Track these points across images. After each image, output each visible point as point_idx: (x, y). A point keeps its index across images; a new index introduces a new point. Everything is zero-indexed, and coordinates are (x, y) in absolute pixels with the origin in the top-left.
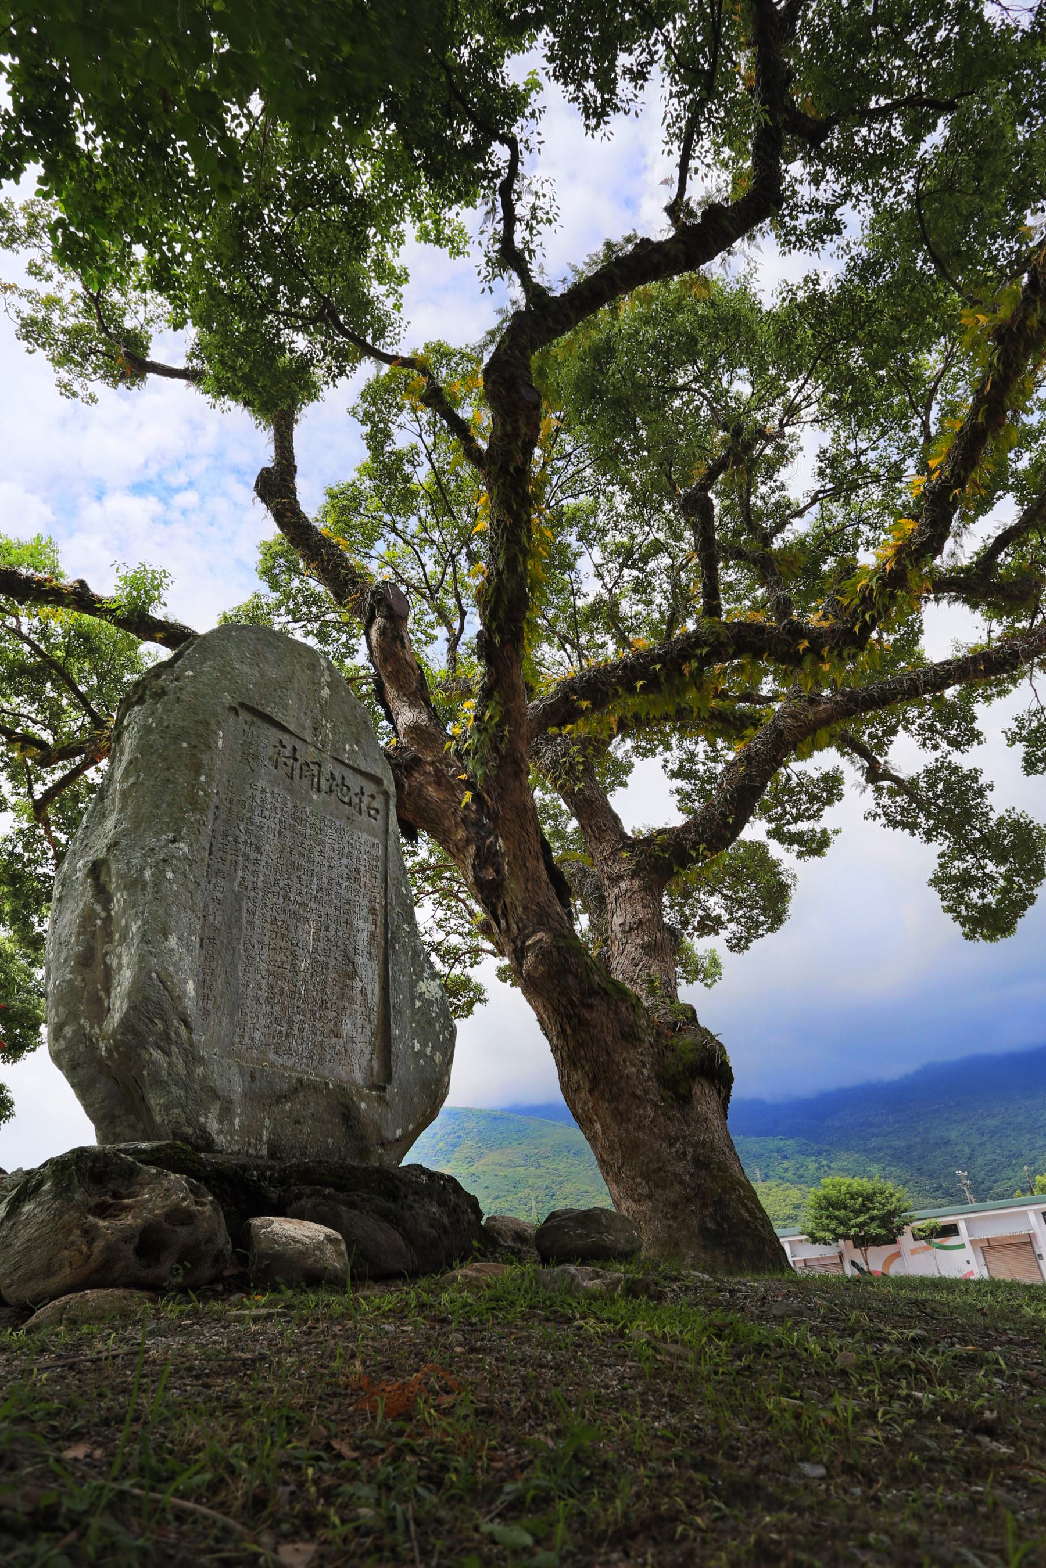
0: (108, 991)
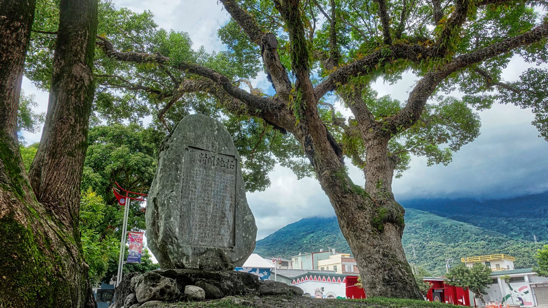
0: (158, 231)
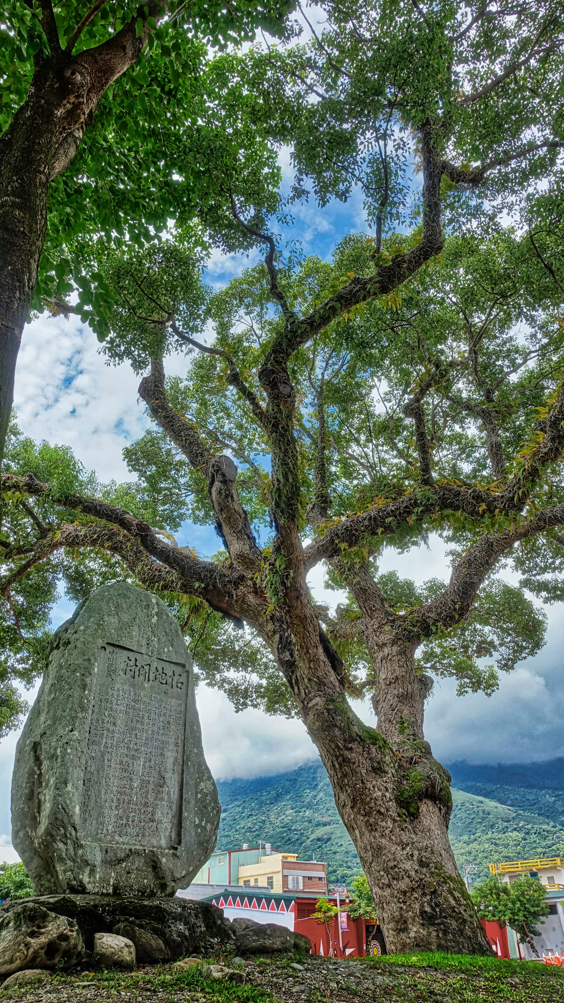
0: (39, 812)
